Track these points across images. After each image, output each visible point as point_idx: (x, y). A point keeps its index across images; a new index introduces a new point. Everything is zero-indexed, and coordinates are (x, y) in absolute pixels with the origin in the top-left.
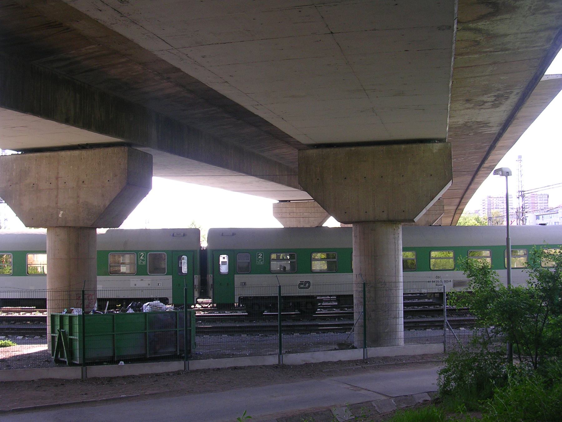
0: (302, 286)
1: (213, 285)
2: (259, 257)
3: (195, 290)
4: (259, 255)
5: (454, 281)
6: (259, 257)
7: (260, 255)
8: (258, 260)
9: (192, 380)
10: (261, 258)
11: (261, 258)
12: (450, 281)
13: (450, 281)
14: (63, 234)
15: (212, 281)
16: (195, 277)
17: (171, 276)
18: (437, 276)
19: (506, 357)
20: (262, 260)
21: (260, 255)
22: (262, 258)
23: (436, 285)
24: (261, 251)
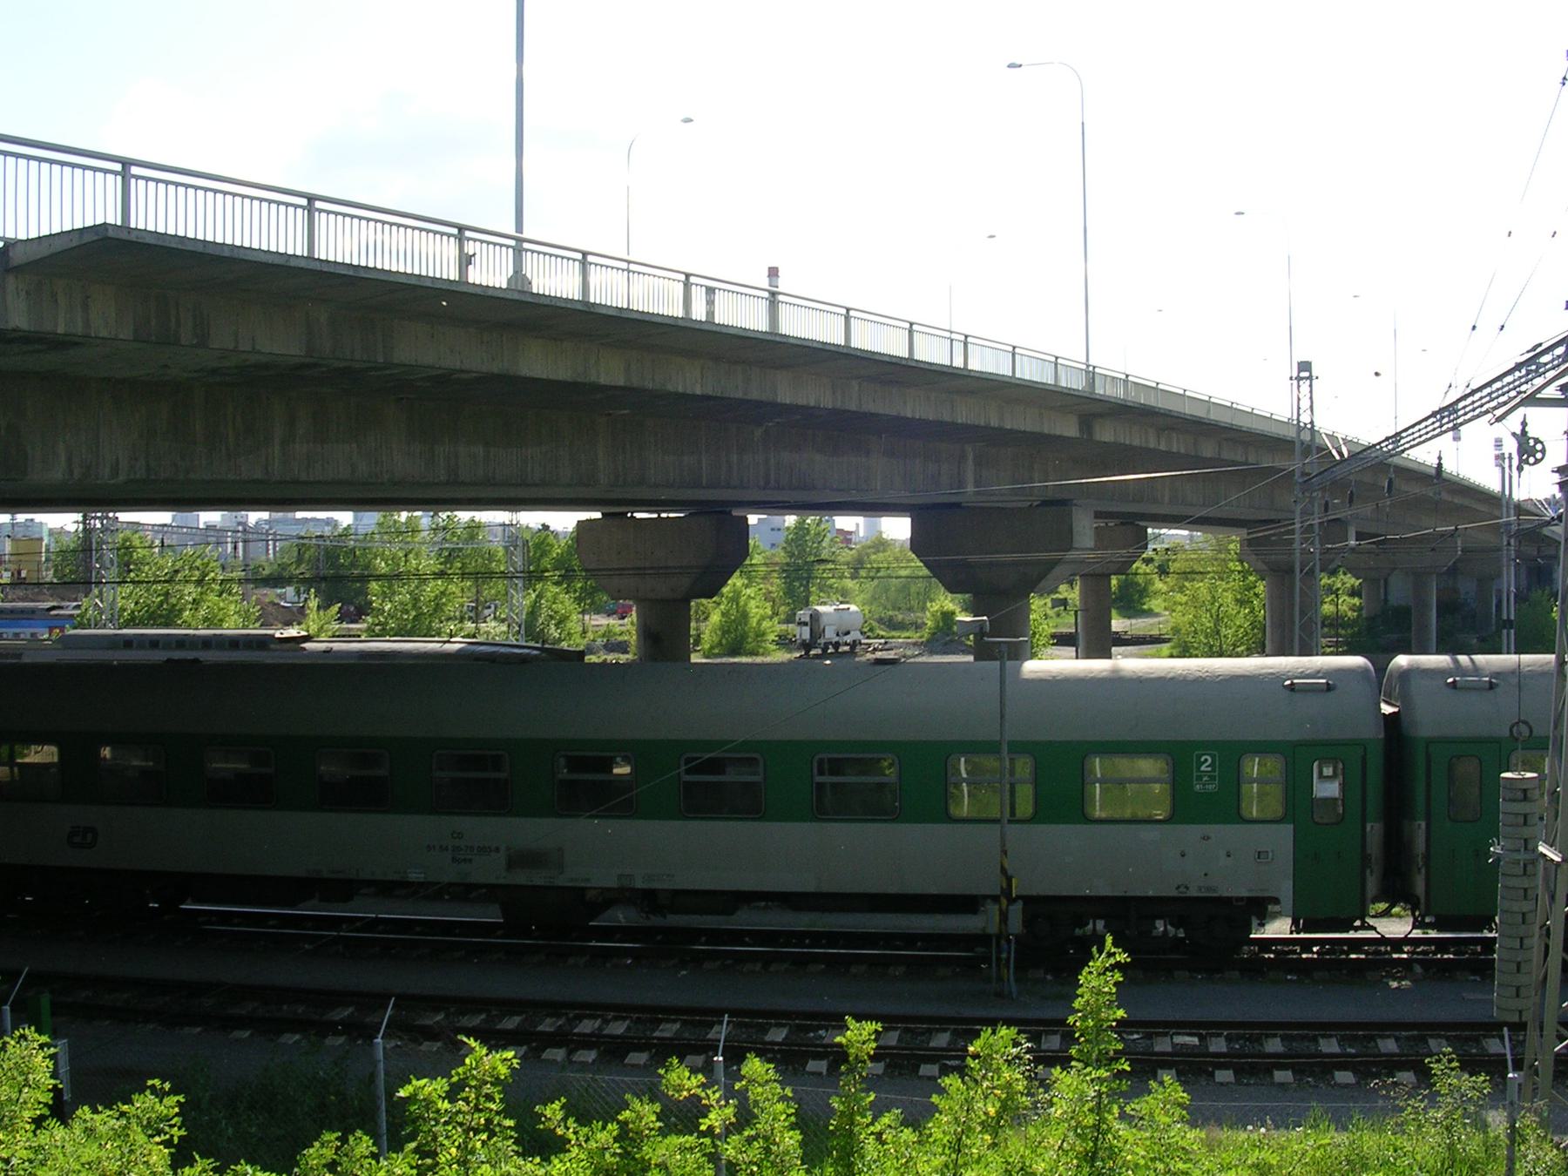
0: (77, 839)
1: (1427, 857)
2: (1203, 768)
3: (1368, 871)
4: (1203, 759)
5: (508, 849)
6: (1203, 768)
7: (1206, 760)
8: (1199, 778)
9: (145, 1159)
10: (1209, 769)
11: (1209, 769)
12: (497, 850)
13: (497, 850)
14: (1516, 666)
15: (1424, 845)
16: (1368, 829)
17: (1292, 826)
18: (454, 832)
19: (65, 1098)
20: (1212, 778)
21: (1206, 760)
22: (1214, 770)
23: (454, 860)
24: (1208, 746)
